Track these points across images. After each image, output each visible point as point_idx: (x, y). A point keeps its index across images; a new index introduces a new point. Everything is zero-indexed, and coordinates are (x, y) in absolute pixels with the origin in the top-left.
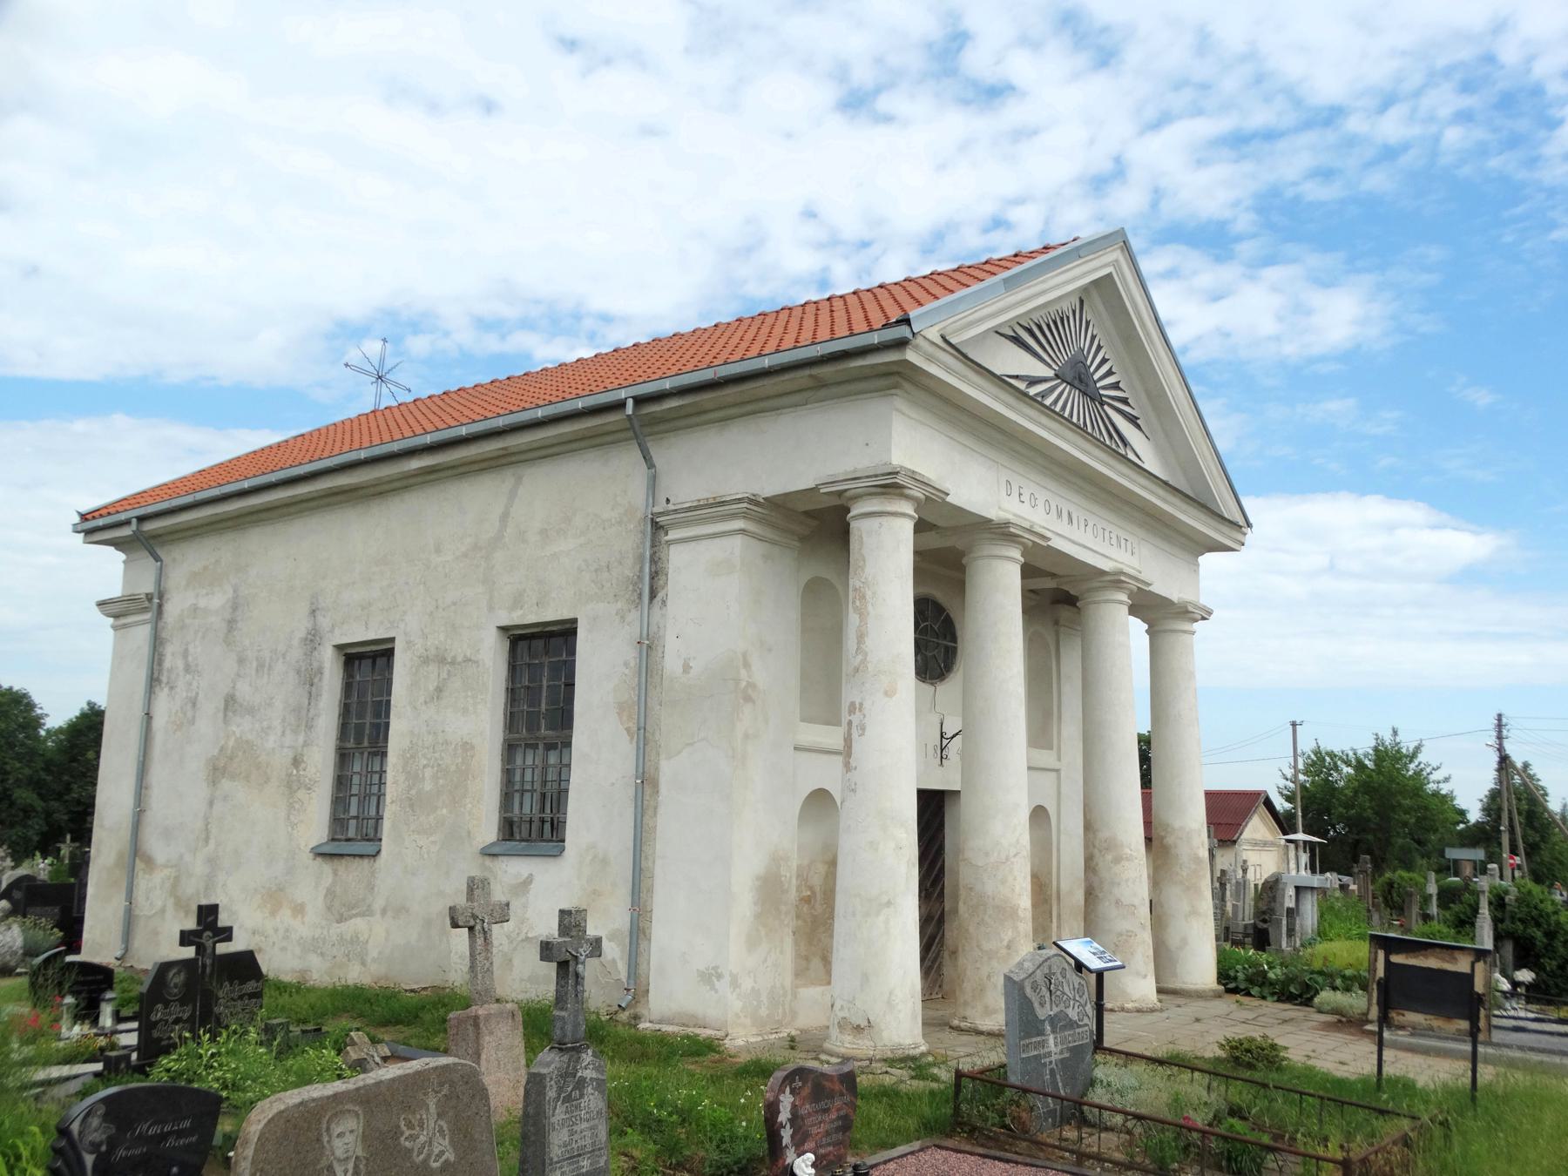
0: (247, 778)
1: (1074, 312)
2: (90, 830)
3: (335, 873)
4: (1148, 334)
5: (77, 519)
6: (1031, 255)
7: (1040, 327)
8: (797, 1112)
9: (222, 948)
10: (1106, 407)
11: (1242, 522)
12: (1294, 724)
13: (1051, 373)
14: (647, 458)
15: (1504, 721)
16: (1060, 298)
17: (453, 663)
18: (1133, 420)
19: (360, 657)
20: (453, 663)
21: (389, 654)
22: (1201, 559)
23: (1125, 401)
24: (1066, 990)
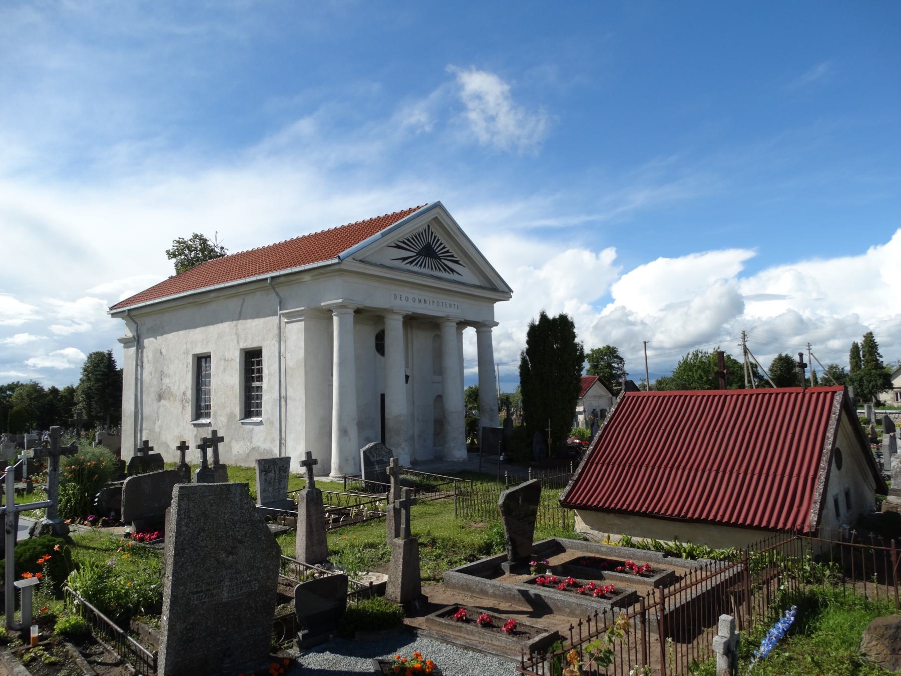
0: (169, 399)
1: (425, 231)
2: (121, 418)
3: (198, 430)
4: (455, 233)
5: (108, 310)
6: (415, 210)
7: (404, 243)
8: (117, 456)
9: (150, 453)
10: (442, 260)
11: (506, 290)
12: (645, 343)
13: (415, 254)
14: (277, 294)
15: (746, 333)
16: (419, 227)
17: (228, 361)
18: (457, 262)
19: (202, 357)
20: (228, 361)
21: (209, 357)
22: (495, 305)
23: (452, 256)
24: (383, 453)
